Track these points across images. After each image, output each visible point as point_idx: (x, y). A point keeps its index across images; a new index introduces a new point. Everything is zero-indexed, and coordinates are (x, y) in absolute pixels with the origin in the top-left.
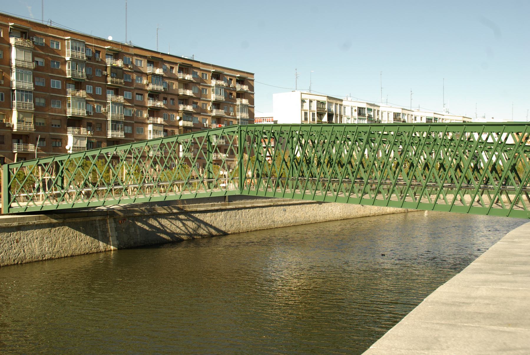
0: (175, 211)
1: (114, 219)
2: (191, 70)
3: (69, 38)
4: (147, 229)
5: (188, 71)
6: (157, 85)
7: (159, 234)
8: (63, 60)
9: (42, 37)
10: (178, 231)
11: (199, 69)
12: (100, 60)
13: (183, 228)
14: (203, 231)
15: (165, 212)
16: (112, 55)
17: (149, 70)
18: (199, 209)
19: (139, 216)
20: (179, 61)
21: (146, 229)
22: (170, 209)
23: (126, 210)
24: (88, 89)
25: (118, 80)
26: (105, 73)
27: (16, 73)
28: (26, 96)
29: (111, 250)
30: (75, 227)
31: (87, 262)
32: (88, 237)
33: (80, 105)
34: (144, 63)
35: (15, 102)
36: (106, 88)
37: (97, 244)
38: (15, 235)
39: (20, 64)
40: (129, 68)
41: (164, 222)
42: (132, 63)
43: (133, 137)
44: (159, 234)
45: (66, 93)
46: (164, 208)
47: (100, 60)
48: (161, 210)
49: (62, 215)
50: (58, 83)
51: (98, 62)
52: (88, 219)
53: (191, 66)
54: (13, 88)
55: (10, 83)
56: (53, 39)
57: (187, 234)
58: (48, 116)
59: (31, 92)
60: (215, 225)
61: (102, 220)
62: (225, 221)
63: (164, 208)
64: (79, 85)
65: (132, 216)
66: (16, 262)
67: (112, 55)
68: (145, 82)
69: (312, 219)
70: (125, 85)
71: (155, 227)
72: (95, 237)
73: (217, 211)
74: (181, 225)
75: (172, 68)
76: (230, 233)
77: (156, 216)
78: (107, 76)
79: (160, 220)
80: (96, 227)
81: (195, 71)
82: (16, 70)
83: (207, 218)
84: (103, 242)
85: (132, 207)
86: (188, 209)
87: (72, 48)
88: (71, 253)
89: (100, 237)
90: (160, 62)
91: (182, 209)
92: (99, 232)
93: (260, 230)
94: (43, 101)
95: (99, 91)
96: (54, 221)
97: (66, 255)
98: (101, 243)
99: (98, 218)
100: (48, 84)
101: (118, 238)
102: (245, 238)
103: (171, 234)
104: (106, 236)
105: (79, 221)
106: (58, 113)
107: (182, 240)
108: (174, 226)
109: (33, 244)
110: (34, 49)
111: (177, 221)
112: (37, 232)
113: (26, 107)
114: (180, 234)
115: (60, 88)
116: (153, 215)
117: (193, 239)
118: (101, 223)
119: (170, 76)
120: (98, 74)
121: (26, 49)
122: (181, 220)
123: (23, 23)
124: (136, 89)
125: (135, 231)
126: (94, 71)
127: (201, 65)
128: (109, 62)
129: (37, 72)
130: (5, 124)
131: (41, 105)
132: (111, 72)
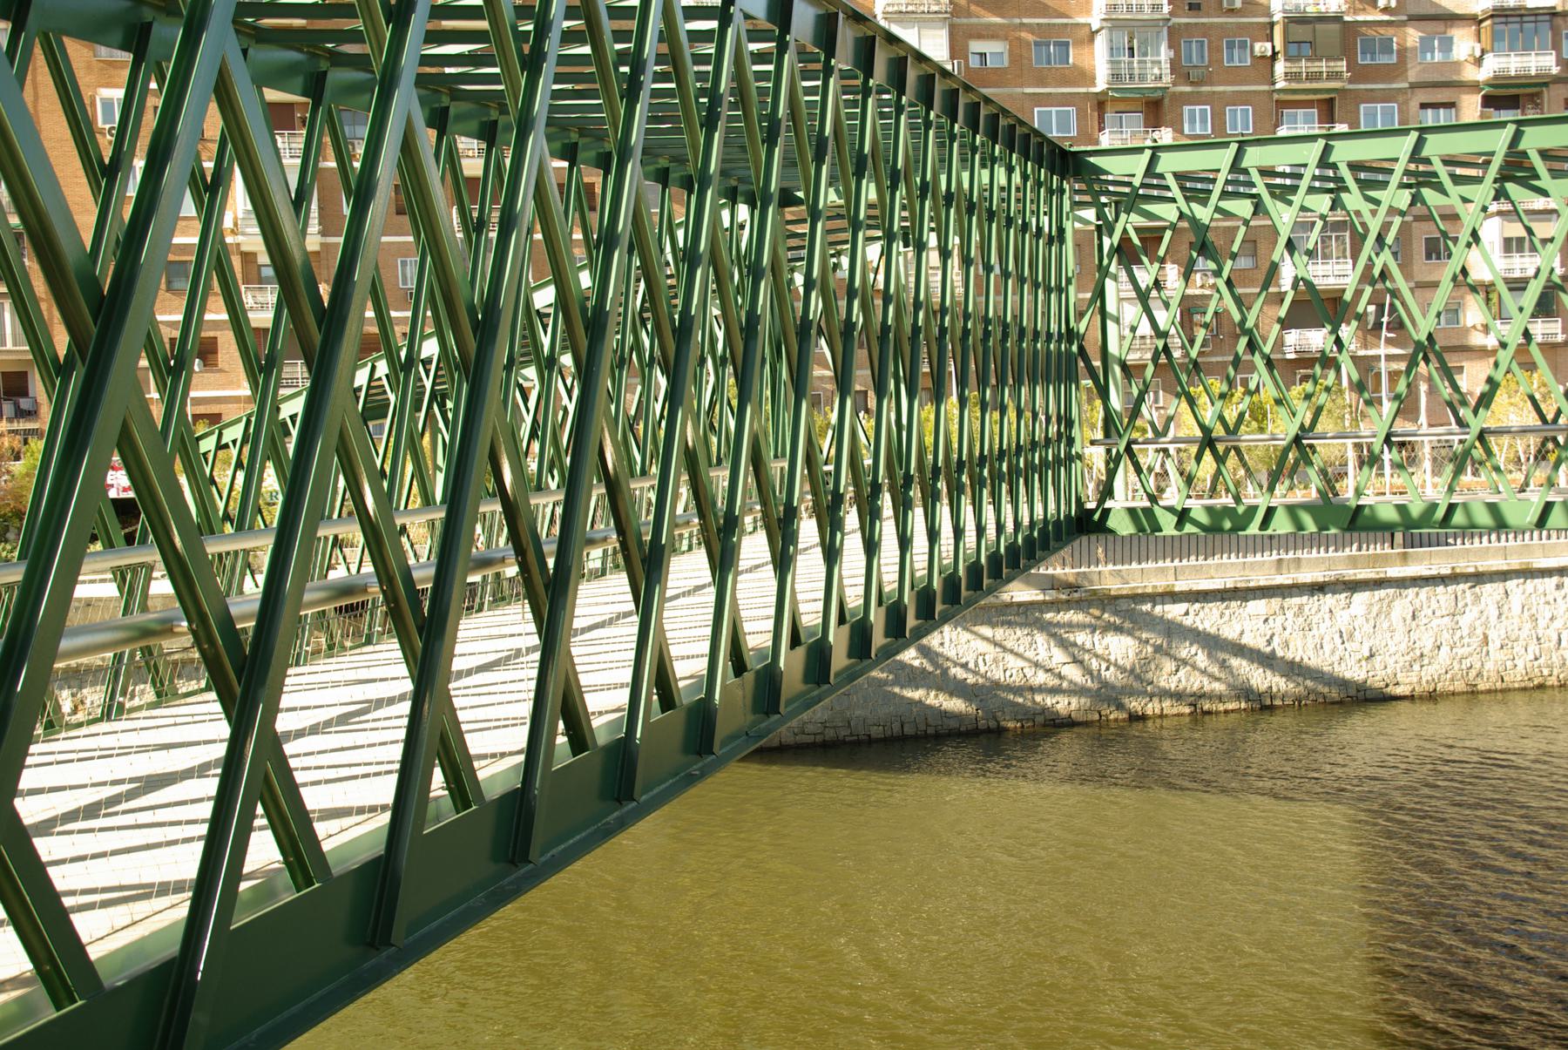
7: (916, 694)
10: (1041, 678)
13: (1074, 673)
14: (1189, 673)
18: (1181, 586)
24: (1192, 121)
25: (1323, 66)
44: (897, 690)
69: (772, 762)
70: (1350, 81)
73: (1319, 588)
74: (1059, 656)
76: (1399, 691)
86: (1113, 586)
91: (1073, 587)
102: (285, 841)
114: (1041, 689)
121: (924, 20)
122: (1045, 627)
124: (1413, 86)
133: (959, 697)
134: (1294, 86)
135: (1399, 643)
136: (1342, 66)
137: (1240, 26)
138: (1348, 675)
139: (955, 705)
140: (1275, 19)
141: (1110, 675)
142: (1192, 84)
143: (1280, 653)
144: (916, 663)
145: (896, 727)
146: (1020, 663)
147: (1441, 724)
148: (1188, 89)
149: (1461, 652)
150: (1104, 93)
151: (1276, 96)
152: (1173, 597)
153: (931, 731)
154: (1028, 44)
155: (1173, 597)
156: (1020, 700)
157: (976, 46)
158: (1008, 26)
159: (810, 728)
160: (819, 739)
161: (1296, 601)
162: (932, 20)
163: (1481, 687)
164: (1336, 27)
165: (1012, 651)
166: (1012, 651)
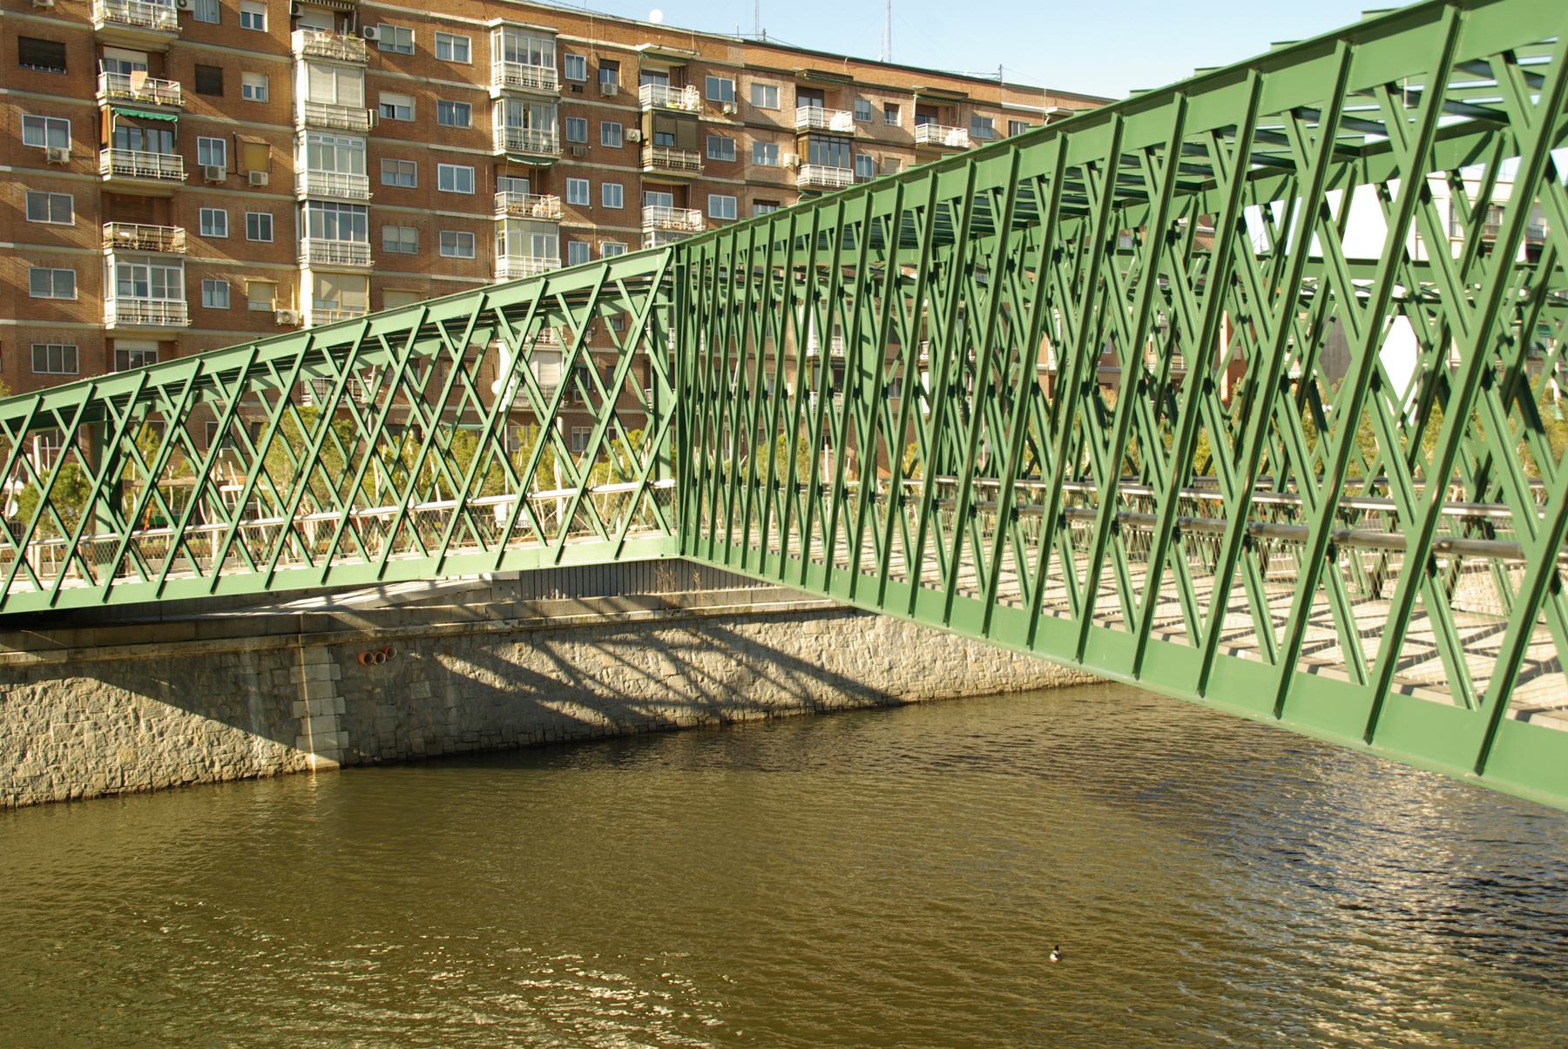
0: (639, 614)
1: (332, 648)
2: (967, 114)
3: (499, 21)
4: (498, 685)
5: (954, 116)
6: (832, 165)
7: (554, 705)
8: (485, 97)
9: (406, 24)
10: (652, 690)
11: (997, 107)
12: (614, 92)
13: (678, 683)
14: (772, 689)
15: (592, 617)
16: (665, 75)
17: (801, 117)
18: (757, 607)
19: (458, 635)
20: (918, 83)
21: (490, 687)
22: (615, 606)
23: (399, 613)
24: (574, 193)
25: (682, 157)
26: (634, 134)
27: (310, 146)
28: (345, 222)
29: (307, 771)
30: (139, 680)
32: (197, 719)
33: (538, 241)
34: (785, 93)
35: (306, 244)
36: (642, 188)
37: (241, 748)
39: (323, 116)
40: (728, 115)
41: (585, 657)
42: (738, 96)
43: (842, 359)
44: (554, 705)
45: (492, 207)
46: (586, 605)
47: (614, 92)
48: (560, 608)
49: (65, 636)
50: (463, 176)
51: (608, 98)
52: (196, 649)
53: (963, 99)
54: (301, 198)
55: (292, 179)
56: (446, 30)
57: (693, 704)
58: (427, 287)
59: (359, 207)
60: (839, 666)
61: (271, 652)
62: (888, 652)
63: (586, 605)
64: (541, 179)
65: (426, 637)
67: (665, 75)
68: (786, 157)
70: (705, 173)
71: (539, 679)
72: (230, 721)
74: (666, 668)
75: (891, 109)
76: (910, 697)
77: (542, 634)
78: (642, 144)
79: (555, 646)
80: (238, 681)
81: (982, 114)
82: (310, 138)
83: (803, 641)
84: (269, 736)
85: (439, 601)
86: (708, 608)
87: (510, 55)
88: (100, 785)
89: (256, 720)
90: (845, 91)
91: (676, 608)
92: (253, 701)
93: (1062, 687)
94: (409, 236)
95: (614, 197)
97: (75, 792)
98: (259, 744)
99: (248, 645)
100: (428, 176)
103: (616, 704)
104: (286, 714)
105: (152, 655)
106: (466, 274)
107: (674, 729)
108: (638, 675)
110: (372, 64)
111: (650, 654)
113: (344, 259)
114: (661, 702)
115: (472, 191)
116: (531, 631)
117: (715, 728)
118: (267, 663)
119: (881, 137)
120: (612, 141)
121: (342, 67)
122: (662, 647)
124: (750, 184)
125: (437, 694)
126: (594, 130)
127: (1004, 92)
128: (648, 95)
129: (382, 141)
130: (273, 315)
131: (408, 250)
132: (654, 131)
133: (589, 706)
134: (660, 171)
135: (906, 659)
136: (698, 158)
137: (615, 113)
138: (875, 685)
139: (585, 714)
140: (644, 109)
141: (714, 690)
142: (574, 158)
143: (827, 667)
144: (554, 676)
145: (539, 736)
146: (637, 675)
147: (938, 722)
148: (571, 162)
149: (949, 664)
150: (500, 157)
151: (643, 178)
152: (750, 617)
153: (567, 737)
154: (433, 103)
155: (750, 617)
156: (644, 712)
157: (386, 98)
158: (416, 83)
159: (468, 737)
160: (476, 746)
161: (836, 622)
162: (350, 68)
163: (964, 693)
164: (693, 124)
165: (629, 665)
166: (629, 665)
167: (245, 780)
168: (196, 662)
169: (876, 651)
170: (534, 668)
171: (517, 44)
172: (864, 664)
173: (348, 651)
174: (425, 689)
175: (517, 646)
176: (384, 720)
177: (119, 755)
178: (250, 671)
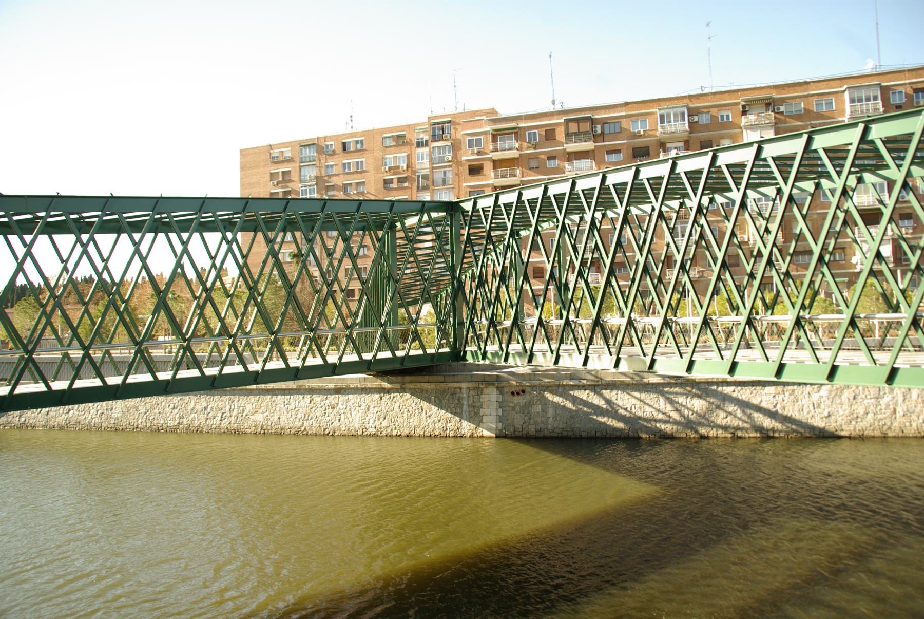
3: (846, 87)
9: (798, 100)
29: (482, 437)
31: (434, 449)
38: (332, 399)
58: (815, 216)
61: (474, 389)
66: (327, 432)
72: (455, 414)
76: (843, 433)
88: (407, 432)
92: (465, 407)
96: (386, 385)
101: (501, 419)
104: (477, 414)
109: (353, 413)
112: (366, 399)
116: (595, 386)
118: (472, 393)
123: (764, 91)
138: (815, 424)
146: (651, 410)
149: (879, 416)
159: (557, 430)
163: (890, 434)
167: (458, 437)
168: (444, 391)
169: (819, 406)
170: (594, 402)
171: (856, 95)
172: (808, 413)
173: (506, 390)
174: (539, 408)
175: (587, 392)
176: (518, 421)
177: (414, 422)
178: (465, 395)
